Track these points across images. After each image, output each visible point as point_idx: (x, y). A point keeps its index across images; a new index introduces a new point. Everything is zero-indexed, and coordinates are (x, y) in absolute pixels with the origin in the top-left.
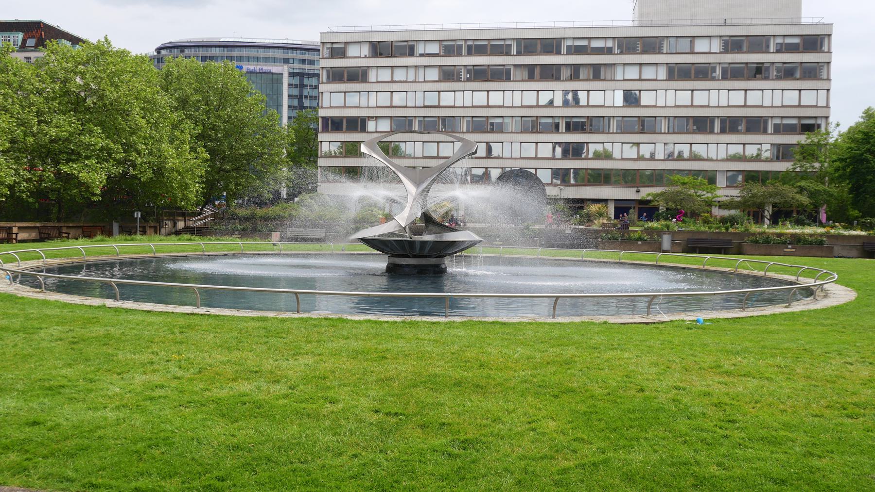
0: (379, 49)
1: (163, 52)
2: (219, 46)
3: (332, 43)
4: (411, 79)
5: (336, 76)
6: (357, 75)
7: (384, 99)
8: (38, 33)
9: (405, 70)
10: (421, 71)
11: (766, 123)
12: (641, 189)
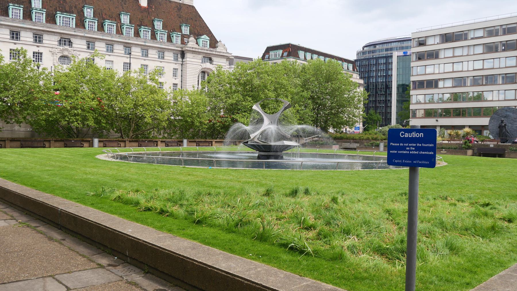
0: (447, 38)
1: (365, 49)
2: (398, 41)
3: (419, 38)
4: (465, 54)
5: (420, 57)
6: (433, 55)
7: (449, 68)
8: (291, 50)
9: (461, 49)
10: (472, 48)
11: (465, 80)
12: (439, 119)
